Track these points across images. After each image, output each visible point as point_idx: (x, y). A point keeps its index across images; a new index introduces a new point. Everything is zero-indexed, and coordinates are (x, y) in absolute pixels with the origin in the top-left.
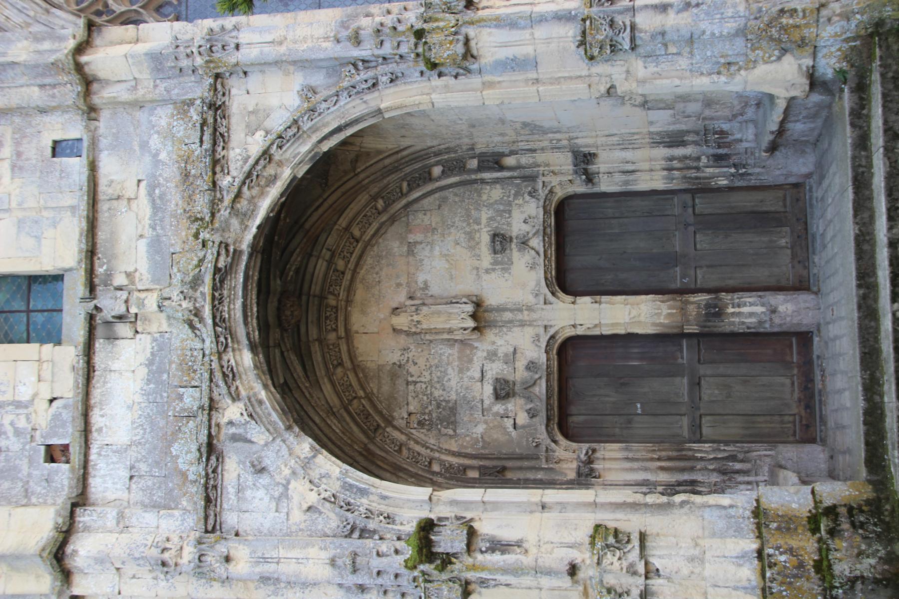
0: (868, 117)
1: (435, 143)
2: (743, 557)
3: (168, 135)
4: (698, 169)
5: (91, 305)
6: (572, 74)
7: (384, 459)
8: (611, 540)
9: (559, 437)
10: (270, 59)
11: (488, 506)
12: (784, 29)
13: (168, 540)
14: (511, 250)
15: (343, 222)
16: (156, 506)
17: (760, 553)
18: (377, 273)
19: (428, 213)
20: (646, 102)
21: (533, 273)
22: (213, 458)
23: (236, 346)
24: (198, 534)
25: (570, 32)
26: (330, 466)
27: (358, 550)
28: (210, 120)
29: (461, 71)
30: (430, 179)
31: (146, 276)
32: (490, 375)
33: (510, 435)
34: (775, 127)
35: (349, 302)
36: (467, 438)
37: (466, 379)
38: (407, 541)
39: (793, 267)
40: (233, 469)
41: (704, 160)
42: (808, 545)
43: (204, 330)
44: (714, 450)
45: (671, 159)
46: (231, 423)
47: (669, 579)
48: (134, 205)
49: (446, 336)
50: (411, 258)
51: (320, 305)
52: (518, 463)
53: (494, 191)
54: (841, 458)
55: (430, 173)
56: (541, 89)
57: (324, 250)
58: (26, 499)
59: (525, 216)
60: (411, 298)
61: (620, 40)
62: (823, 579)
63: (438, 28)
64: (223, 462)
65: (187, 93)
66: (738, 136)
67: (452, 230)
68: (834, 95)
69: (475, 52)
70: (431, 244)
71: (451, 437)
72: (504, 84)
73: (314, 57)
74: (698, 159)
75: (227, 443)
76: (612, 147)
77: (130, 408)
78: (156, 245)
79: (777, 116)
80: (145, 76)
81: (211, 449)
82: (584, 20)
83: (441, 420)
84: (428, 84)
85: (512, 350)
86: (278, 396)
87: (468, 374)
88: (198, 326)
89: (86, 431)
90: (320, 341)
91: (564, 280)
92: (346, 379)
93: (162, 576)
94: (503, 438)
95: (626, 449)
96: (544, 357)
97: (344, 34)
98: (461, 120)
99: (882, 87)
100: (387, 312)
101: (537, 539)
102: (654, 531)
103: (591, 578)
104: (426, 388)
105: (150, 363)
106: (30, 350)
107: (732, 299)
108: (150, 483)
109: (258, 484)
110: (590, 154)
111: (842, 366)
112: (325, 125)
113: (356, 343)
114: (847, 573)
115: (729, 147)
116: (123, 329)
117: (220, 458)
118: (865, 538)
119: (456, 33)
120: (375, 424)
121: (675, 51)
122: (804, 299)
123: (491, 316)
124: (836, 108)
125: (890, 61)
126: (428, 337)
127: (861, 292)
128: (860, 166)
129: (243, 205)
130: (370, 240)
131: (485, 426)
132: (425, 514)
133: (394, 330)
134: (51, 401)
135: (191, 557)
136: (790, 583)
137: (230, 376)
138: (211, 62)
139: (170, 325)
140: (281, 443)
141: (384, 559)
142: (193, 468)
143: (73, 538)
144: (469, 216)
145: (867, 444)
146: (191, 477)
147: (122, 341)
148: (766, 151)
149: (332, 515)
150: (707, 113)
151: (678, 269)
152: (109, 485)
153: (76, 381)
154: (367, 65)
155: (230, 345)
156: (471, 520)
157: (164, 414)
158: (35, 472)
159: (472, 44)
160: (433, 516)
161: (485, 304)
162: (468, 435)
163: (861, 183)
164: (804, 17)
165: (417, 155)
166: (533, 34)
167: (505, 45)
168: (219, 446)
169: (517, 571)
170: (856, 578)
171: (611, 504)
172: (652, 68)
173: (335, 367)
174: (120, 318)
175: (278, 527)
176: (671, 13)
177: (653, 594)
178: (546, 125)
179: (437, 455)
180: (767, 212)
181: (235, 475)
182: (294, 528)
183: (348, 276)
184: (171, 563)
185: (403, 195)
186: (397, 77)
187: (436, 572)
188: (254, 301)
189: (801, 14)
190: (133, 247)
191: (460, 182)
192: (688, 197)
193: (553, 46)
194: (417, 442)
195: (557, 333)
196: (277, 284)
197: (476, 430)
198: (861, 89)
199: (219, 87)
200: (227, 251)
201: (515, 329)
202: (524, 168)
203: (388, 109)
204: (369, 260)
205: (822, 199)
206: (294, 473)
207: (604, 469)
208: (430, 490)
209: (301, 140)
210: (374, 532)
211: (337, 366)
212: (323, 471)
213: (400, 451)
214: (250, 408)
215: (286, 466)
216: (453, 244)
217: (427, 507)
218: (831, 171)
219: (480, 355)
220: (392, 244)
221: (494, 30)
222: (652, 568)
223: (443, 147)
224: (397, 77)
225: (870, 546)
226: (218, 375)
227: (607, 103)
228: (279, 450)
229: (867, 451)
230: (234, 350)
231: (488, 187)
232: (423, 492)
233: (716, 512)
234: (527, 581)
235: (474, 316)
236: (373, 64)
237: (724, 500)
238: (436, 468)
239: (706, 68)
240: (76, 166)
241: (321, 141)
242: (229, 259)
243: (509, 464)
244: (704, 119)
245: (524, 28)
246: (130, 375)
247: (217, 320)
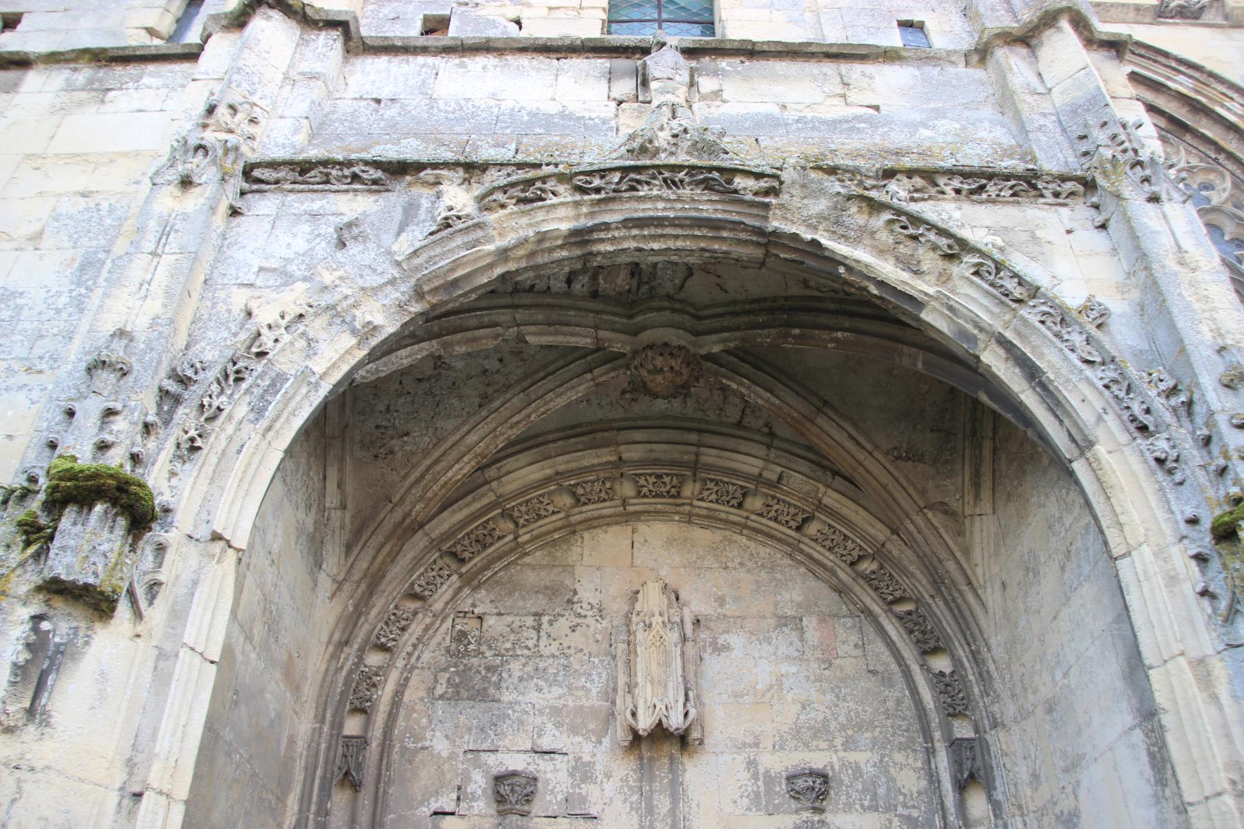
14: (797, 811)
15: (831, 499)
18: (741, 564)
19: (859, 652)
22: (379, 174)
23: (585, 210)
26: (333, 357)
27: (130, 379)
29: (1223, 604)
32: (543, 766)
33: (422, 803)
35: (689, 519)
36: (424, 720)
37: (539, 720)
50: (772, 622)
51: (681, 464)
53: (913, 775)
55: (936, 650)
57: (779, 469)
60: (697, 622)
64: (369, 191)
67: (830, 697)
70: (801, 658)
71: (431, 690)
73: (1175, 311)
78: (772, 123)
85: (593, 811)
86: (484, 280)
87: (550, 726)
92: (550, 508)
94: (417, 788)
98: (1066, 675)
101: (39, 764)
104: (527, 648)
109: (318, 240)
120: (467, 555)
123: (662, 771)
129: (856, 216)
131: (445, 754)
140: (388, 277)
144: (859, 727)
147: (606, 86)
154: (1182, 412)
155: (586, 197)
161: (686, 759)
162: (430, 722)
165: (970, 619)
179: (400, 663)
186: (1170, 472)
188: (671, 244)
191: (924, 709)
199: (1069, 186)
200: (767, 192)
201: (636, 817)
203: (1095, 469)
209: (996, 310)
211: (574, 494)
212: (322, 346)
215: (341, 278)
216: (803, 698)
219: (586, 749)
220: (798, 589)
223: (992, 667)
224: (1170, 472)
226: (531, 174)
228: (374, 270)
230: (577, 204)
231: (919, 764)
238: (374, 659)
241: (1003, 342)
242: (749, 197)
247: (632, 175)
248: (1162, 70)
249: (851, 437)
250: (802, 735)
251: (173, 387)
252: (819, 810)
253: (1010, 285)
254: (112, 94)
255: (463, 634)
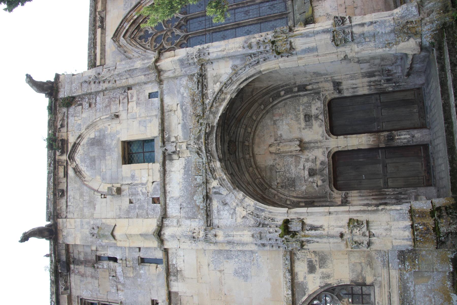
0: (444, 59)
1: (281, 83)
2: (406, 228)
3: (186, 87)
4: (380, 85)
5: (164, 148)
6: (330, 52)
7: (269, 200)
8: (356, 224)
9: (334, 189)
10: (220, 57)
11: (309, 214)
12: (409, 29)
13: (195, 229)
15: (249, 114)
16: (189, 218)
17: (412, 226)
20: (359, 61)
21: (321, 128)
24: (205, 227)
25: (328, 37)
26: (250, 201)
27: (262, 231)
28: (201, 80)
30: (280, 96)
31: (182, 137)
34: (408, 66)
35: (253, 143)
38: (280, 228)
39: (420, 120)
40: (215, 204)
41: (383, 81)
42: (430, 222)
43: (203, 155)
44: (393, 191)
45: (370, 82)
46: (214, 188)
47: (378, 237)
48: (176, 113)
49: (290, 154)
50: (275, 126)
52: (319, 200)
54: (442, 190)
55: (280, 94)
56: (319, 58)
58: (147, 216)
59: (317, 107)
60: (276, 140)
61: (347, 38)
62: (436, 234)
63: (280, 39)
65: (192, 72)
66: (395, 71)
67: (290, 114)
68: (430, 52)
69: (294, 47)
70: (282, 120)
71: (293, 191)
72: (306, 58)
74: (380, 81)
75: (213, 195)
76: (347, 79)
77: (179, 184)
78: (184, 126)
79: (409, 62)
80: (178, 67)
81: (207, 198)
82: (333, 32)
83: (289, 185)
84: (277, 60)
85: (314, 157)
88: (201, 153)
89: (165, 192)
90: (244, 158)
91: (333, 130)
93: (193, 242)
95: (360, 192)
96: (327, 160)
97: (246, 45)
99: (448, 47)
100: (267, 146)
102: (372, 220)
103: (348, 238)
105: (185, 168)
106: (145, 165)
107: (397, 133)
108: (187, 210)
110: (339, 82)
111: (441, 155)
112: (241, 78)
113: (256, 158)
114: (445, 231)
115: (392, 76)
116: (175, 156)
117: (211, 200)
118: (452, 218)
119: (287, 41)
121: (368, 40)
122: (425, 131)
123: (306, 145)
124: (431, 57)
125: (450, 37)
126: (283, 154)
127: (446, 125)
128: (442, 77)
129: (214, 109)
130: (259, 120)
132: (286, 218)
133: (270, 153)
134: (153, 182)
135: (203, 235)
136: (424, 236)
137: (213, 171)
138: (200, 60)
139: (191, 154)
141: (272, 234)
142: (202, 204)
143: (163, 229)
144: (295, 109)
145: (451, 183)
146: (201, 207)
148: (406, 76)
149: (252, 219)
150: (382, 63)
151: (376, 123)
152: (174, 211)
153: (160, 175)
156: (303, 219)
157: (190, 185)
158: (150, 207)
159: (293, 44)
160: (288, 218)
163: (443, 84)
164: (416, 24)
166: (315, 38)
167: (305, 44)
168: (210, 196)
169: (321, 237)
170: (449, 233)
171: (355, 211)
172: (360, 47)
173: (249, 167)
174: (174, 152)
175: (233, 224)
176: (366, 27)
177: (372, 243)
178: (322, 72)
180: (408, 100)
181: (216, 206)
182: (238, 224)
183: (252, 134)
184: (196, 237)
185: (271, 103)
187: (291, 238)
189: (415, 23)
190: (177, 130)
192: (377, 96)
193: (323, 42)
194: (281, 194)
195: (331, 150)
196: (227, 138)
197: (303, 188)
198: (440, 49)
199: (203, 68)
200: (209, 126)
202: (315, 89)
203: (264, 71)
204: (259, 128)
205: (429, 93)
206: (237, 205)
207: (352, 200)
208: (287, 209)
210: (268, 225)
212: (248, 204)
213: (274, 197)
214: (219, 182)
217: (286, 215)
218: (431, 81)
219: (303, 160)
220: (268, 121)
221: (300, 39)
222: (371, 233)
225: (454, 221)
226: (208, 171)
227: (344, 63)
229: (451, 186)
230: (213, 162)
232: (285, 210)
233: (395, 212)
234: (325, 240)
235: (299, 146)
236: (257, 55)
237: (398, 207)
239: (380, 46)
240: (156, 101)
243: (316, 200)
244: (382, 66)
245: (311, 37)
246: (178, 172)
248: (122, 30)
249: (239, 110)
250: (297, 119)
251: (261, 226)
252: (312, 116)
253: (229, 82)
254: (178, 269)
255: (281, 186)
